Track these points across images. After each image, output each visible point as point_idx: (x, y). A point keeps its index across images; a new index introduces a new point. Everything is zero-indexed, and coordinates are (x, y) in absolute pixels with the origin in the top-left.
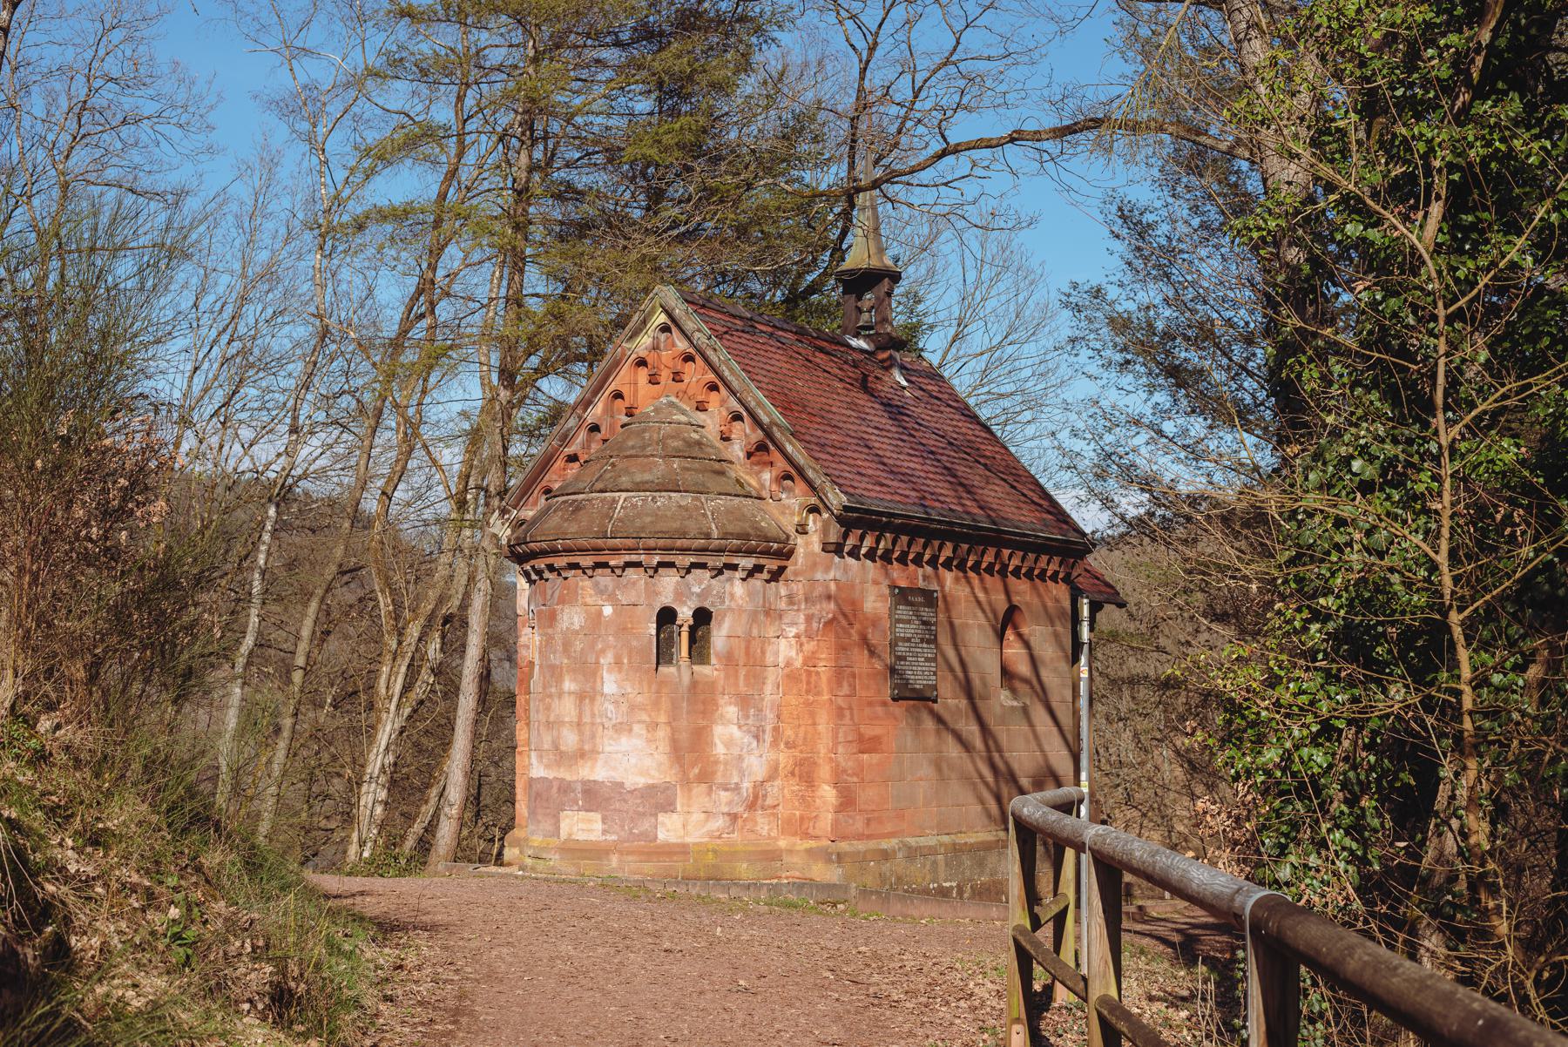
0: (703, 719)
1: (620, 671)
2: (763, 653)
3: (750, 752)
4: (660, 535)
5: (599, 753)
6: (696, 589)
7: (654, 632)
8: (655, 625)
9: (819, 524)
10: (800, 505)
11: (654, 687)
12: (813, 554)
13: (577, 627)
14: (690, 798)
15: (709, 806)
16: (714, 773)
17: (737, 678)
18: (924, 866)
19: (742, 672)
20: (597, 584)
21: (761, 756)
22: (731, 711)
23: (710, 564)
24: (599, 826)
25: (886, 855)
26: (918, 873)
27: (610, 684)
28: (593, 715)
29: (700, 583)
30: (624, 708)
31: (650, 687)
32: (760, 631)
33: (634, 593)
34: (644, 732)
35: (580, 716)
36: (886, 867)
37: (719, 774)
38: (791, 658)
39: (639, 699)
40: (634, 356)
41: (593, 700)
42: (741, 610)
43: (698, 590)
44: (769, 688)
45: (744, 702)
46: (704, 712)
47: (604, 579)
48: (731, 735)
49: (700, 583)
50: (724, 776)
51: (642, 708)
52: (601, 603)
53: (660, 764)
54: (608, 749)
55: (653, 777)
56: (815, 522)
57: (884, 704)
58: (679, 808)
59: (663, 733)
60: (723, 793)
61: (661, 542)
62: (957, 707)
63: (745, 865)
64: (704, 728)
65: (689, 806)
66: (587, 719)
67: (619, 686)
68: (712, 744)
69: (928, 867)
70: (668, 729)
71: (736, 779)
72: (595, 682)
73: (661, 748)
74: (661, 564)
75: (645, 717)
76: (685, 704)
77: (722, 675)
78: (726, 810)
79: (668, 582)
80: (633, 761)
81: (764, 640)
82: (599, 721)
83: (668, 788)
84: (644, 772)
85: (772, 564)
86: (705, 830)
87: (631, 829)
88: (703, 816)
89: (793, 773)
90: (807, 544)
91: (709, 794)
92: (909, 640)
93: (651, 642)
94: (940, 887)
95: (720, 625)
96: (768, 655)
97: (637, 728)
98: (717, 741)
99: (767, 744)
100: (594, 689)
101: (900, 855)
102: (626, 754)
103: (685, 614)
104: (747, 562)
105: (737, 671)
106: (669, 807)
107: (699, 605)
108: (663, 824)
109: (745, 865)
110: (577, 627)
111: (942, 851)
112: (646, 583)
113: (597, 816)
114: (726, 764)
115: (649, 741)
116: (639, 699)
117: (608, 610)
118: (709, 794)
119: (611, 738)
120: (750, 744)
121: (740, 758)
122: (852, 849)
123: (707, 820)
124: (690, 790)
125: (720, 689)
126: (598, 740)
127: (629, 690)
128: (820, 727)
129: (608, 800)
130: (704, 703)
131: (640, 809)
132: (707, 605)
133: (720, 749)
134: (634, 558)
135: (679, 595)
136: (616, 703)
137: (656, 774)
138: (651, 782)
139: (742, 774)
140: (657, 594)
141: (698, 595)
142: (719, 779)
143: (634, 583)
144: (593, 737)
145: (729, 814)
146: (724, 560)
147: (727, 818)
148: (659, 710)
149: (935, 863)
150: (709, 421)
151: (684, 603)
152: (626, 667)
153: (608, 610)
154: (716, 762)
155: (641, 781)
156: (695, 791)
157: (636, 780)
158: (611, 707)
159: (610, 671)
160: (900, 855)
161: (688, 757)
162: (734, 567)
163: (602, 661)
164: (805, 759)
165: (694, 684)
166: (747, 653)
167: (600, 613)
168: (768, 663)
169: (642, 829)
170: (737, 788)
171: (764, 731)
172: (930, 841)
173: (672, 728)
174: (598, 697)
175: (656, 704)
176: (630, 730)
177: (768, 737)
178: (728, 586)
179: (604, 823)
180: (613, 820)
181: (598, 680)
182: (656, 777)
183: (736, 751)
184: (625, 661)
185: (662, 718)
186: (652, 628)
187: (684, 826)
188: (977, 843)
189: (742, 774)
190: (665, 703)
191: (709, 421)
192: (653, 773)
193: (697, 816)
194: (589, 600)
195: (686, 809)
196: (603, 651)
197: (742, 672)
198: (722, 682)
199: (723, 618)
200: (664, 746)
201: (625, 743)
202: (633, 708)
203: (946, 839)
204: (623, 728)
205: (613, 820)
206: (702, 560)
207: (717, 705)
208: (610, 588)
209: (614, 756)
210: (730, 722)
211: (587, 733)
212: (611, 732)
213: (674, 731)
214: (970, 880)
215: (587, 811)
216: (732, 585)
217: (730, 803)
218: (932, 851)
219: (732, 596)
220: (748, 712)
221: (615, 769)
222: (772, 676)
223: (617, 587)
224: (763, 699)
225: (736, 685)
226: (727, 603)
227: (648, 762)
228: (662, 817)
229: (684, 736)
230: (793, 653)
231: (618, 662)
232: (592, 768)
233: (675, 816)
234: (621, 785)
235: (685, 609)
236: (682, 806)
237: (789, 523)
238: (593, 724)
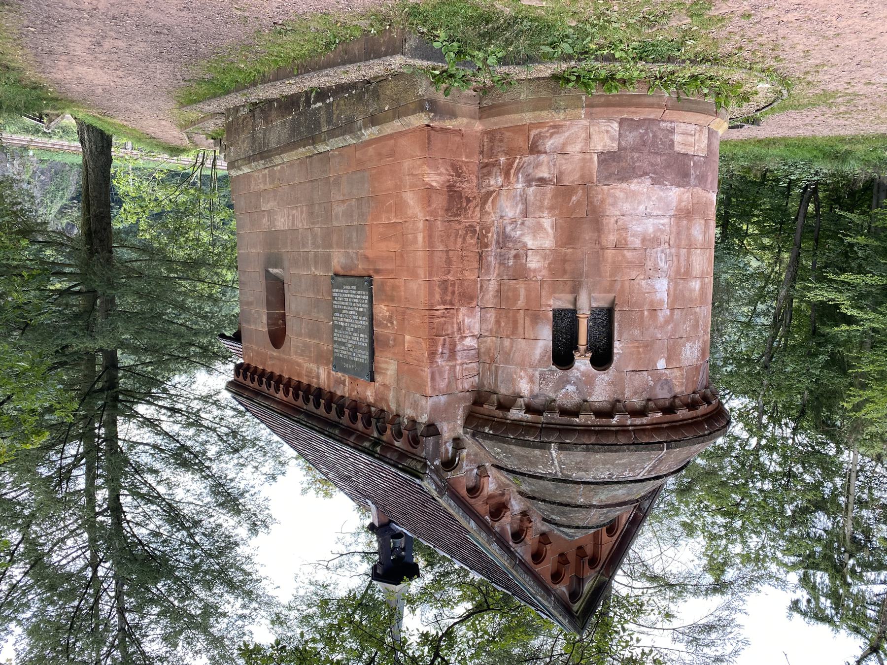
0: (566, 254)
1: (652, 303)
2: (498, 322)
3: (513, 221)
4: (614, 448)
5: (674, 216)
6: (571, 388)
7: (616, 344)
8: (615, 351)
9: (443, 450)
10: (461, 468)
11: (618, 286)
12: (447, 420)
13: (688, 345)
14: (582, 168)
15: (561, 160)
16: (555, 196)
17: (528, 297)
18: (338, 118)
19: (521, 303)
20: (670, 389)
21: (501, 217)
22: (534, 263)
23: (557, 416)
24: (677, 138)
25: (373, 121)
26: (342, 113)
27: (662, 287)
28: (678, 256)
29: (566, 394)
30: (649, 264)
31: (622, 286)
32: (501, 343)
33: (636, 383)
34: (630, 239)
35: (689, 254)
36: (373, 108)
37: (549, 196)
38: (469, 317)
39: (633, 274)
40: (598, 569)
41: (678, 272)
42: (522, 366)
43: (568, 387)
44: (492, 286)
45: (521, 273)
46: (564, 261)
47: (663, 394)
48: (535, 237)
49: (566, 394)
50: (544, 194)
51: (631, 264)
52: (667, 372)
53: (614, 205)
54: (665, 221)
55: (622, 190)
56: (447, 450)
57: (377, 271)
58: (595, 156)
59: (611, 238)
60: (546, 175)
61: (612, 440)
62: (316, 268)
63: (523, 96)
64: (564, 245)
65: (584, 159)
66: (683, 251)
67: (653, 287)
68: (555, 227)
69: (335, 116)
70: (604, 243)
71: (531, 191)
72: (675, 290)
73: (613, 220)
74: (609, 414)
75: (628, 254)
76: (586, 269)
77: (543, 301)
78: (543, 157)
79: (600, 395)
80: (642, 208)
81: (496, 333)
82: (673, 250)
83: (607, 178)
84: (632, 196)
85: (489, 409)
86: (567, 134)
87: (647, 133)
88: (569, 149)
89: (468, 200)
90: (454, 429)
91: (561, 173)
92: (356, 330)
93: (620, 334)
94: (323, 101)
95: (546, 351)
96: (493, 319)
97: (637, 243)
98: (550, 231)
99: (494, 229)
100: (676, 284)
101: (360, 123)
102: (648, 216)
103: (582, 364)
104: (516, 414)
105: (527, 303)
106: (606, 158)
107: (568, 372)
108: (612, 139)
109: (523, 96)
110: (688, 345)
111: (323, 136)
112: (623, 394)
113: (678, 148)
114: (541, 208)
115: (625, 229)
116: (633, 274)
117: (661, 364)
118: (561, 173)
119: (662, 232)
120: (513, 230)
121: (525, 214)
122: (406, 119)
123: (564, 145)
124: (582, 177)
125: (545, 285)
126: (674, 229)
127: (643, 283)
128: (441, 248)
129: (668, 166)
130: (565, 272)
131: (636, 155)
132: (559, 373)
133: (547, 223)
134: (638, 421)
135: (589, 381)
136: (657, 269)
137: (619, 194)
138: (624, 185)
139: (524, 200)
140: (612, 383)
141: (568, 382)
142: (549, 189)
143: (635, 393)
144: (678, 233)
145: (539, 152)
146: (542, 419)
147: (542, 148)
148: (614, 262)
149: (329, 122)
150: (539, 525)
151: (584, 374)
152: (646, 307)
153: (661, 364)
154: (551, 208)
155: (634, 185)
156: (577, 176)
157: (640, 186)
158: (662, 265)
159: (661, 302)
160: (360, 123)
161: (581, 213)
162: (529, 409)
163: (668, 312)
164: (456, 215)
165: (575, 291)
166: (515, 322)
167: (668, 360)
168: (493, 311)
169: (635, 133)
170: (529, 182)
171: (498, 242)
172: (337, 142)
173: (599, 243)
174: (673, 274)
175: (617, 268)
176: (644, 240)
177: (492, 237)
178: (536, 389)
179: (672, 141)
180: (663, 143)
181: (672, 292)
182: (619, 190)
183: (529, 221)
184: (646, 313)
185: (610, 254)
186: (617, 348)
187: (590, 137)
188: (296, 149)
189: (524, 200)
190: (607, 269)
191: (539, 525)
192: (621, 195)
193: (575, 148)
194: (677, 373)
195: (588, 156)
196: (667, 322)
197: (521, 303)
198: (544, 293)
199: (542, 357)
200: (610, 223)
201: (649, 226)
202: (641, 265)
203: (322, 148)
204: (650, 242)
205: (663, 143)
206: (565, 419)
207: (550, 269)
208: (658, 387)
209: (660, 213)
210: (536, 252)
211: (684, 237)
212: (664, 237)
213: (598, 241)
214: (301, 113)
215: (687, 154)
216: (531, 391)
217: (538, 165)
218: (331, 134)
219: (531, 380)
220: (515, 264)
221: (660, 199)
222: (489, 298)
223: (652, 388)
224: (498, 275)
225: (528, 290)
226: (537, 374)
227: (626, 207)
228: (614, 146)
229: (588, 235)
230: (467, 320)
231: (653, 311)
232: (680, 201)
233: (599, 148)
234: (655, 182)
235: (583, 368)
236: (591, 159)
237: (471, 446)
238: (678, 247)
